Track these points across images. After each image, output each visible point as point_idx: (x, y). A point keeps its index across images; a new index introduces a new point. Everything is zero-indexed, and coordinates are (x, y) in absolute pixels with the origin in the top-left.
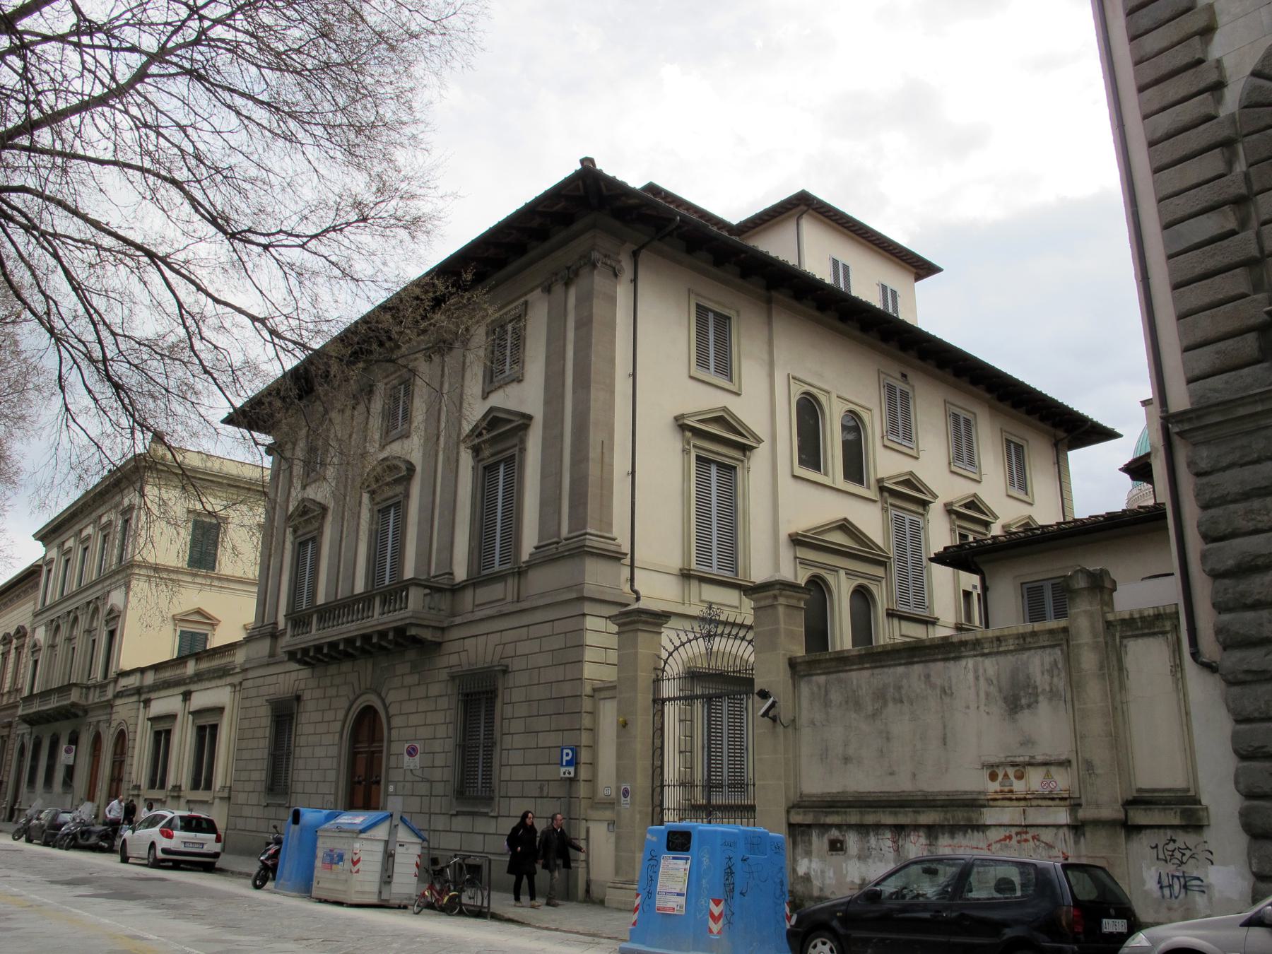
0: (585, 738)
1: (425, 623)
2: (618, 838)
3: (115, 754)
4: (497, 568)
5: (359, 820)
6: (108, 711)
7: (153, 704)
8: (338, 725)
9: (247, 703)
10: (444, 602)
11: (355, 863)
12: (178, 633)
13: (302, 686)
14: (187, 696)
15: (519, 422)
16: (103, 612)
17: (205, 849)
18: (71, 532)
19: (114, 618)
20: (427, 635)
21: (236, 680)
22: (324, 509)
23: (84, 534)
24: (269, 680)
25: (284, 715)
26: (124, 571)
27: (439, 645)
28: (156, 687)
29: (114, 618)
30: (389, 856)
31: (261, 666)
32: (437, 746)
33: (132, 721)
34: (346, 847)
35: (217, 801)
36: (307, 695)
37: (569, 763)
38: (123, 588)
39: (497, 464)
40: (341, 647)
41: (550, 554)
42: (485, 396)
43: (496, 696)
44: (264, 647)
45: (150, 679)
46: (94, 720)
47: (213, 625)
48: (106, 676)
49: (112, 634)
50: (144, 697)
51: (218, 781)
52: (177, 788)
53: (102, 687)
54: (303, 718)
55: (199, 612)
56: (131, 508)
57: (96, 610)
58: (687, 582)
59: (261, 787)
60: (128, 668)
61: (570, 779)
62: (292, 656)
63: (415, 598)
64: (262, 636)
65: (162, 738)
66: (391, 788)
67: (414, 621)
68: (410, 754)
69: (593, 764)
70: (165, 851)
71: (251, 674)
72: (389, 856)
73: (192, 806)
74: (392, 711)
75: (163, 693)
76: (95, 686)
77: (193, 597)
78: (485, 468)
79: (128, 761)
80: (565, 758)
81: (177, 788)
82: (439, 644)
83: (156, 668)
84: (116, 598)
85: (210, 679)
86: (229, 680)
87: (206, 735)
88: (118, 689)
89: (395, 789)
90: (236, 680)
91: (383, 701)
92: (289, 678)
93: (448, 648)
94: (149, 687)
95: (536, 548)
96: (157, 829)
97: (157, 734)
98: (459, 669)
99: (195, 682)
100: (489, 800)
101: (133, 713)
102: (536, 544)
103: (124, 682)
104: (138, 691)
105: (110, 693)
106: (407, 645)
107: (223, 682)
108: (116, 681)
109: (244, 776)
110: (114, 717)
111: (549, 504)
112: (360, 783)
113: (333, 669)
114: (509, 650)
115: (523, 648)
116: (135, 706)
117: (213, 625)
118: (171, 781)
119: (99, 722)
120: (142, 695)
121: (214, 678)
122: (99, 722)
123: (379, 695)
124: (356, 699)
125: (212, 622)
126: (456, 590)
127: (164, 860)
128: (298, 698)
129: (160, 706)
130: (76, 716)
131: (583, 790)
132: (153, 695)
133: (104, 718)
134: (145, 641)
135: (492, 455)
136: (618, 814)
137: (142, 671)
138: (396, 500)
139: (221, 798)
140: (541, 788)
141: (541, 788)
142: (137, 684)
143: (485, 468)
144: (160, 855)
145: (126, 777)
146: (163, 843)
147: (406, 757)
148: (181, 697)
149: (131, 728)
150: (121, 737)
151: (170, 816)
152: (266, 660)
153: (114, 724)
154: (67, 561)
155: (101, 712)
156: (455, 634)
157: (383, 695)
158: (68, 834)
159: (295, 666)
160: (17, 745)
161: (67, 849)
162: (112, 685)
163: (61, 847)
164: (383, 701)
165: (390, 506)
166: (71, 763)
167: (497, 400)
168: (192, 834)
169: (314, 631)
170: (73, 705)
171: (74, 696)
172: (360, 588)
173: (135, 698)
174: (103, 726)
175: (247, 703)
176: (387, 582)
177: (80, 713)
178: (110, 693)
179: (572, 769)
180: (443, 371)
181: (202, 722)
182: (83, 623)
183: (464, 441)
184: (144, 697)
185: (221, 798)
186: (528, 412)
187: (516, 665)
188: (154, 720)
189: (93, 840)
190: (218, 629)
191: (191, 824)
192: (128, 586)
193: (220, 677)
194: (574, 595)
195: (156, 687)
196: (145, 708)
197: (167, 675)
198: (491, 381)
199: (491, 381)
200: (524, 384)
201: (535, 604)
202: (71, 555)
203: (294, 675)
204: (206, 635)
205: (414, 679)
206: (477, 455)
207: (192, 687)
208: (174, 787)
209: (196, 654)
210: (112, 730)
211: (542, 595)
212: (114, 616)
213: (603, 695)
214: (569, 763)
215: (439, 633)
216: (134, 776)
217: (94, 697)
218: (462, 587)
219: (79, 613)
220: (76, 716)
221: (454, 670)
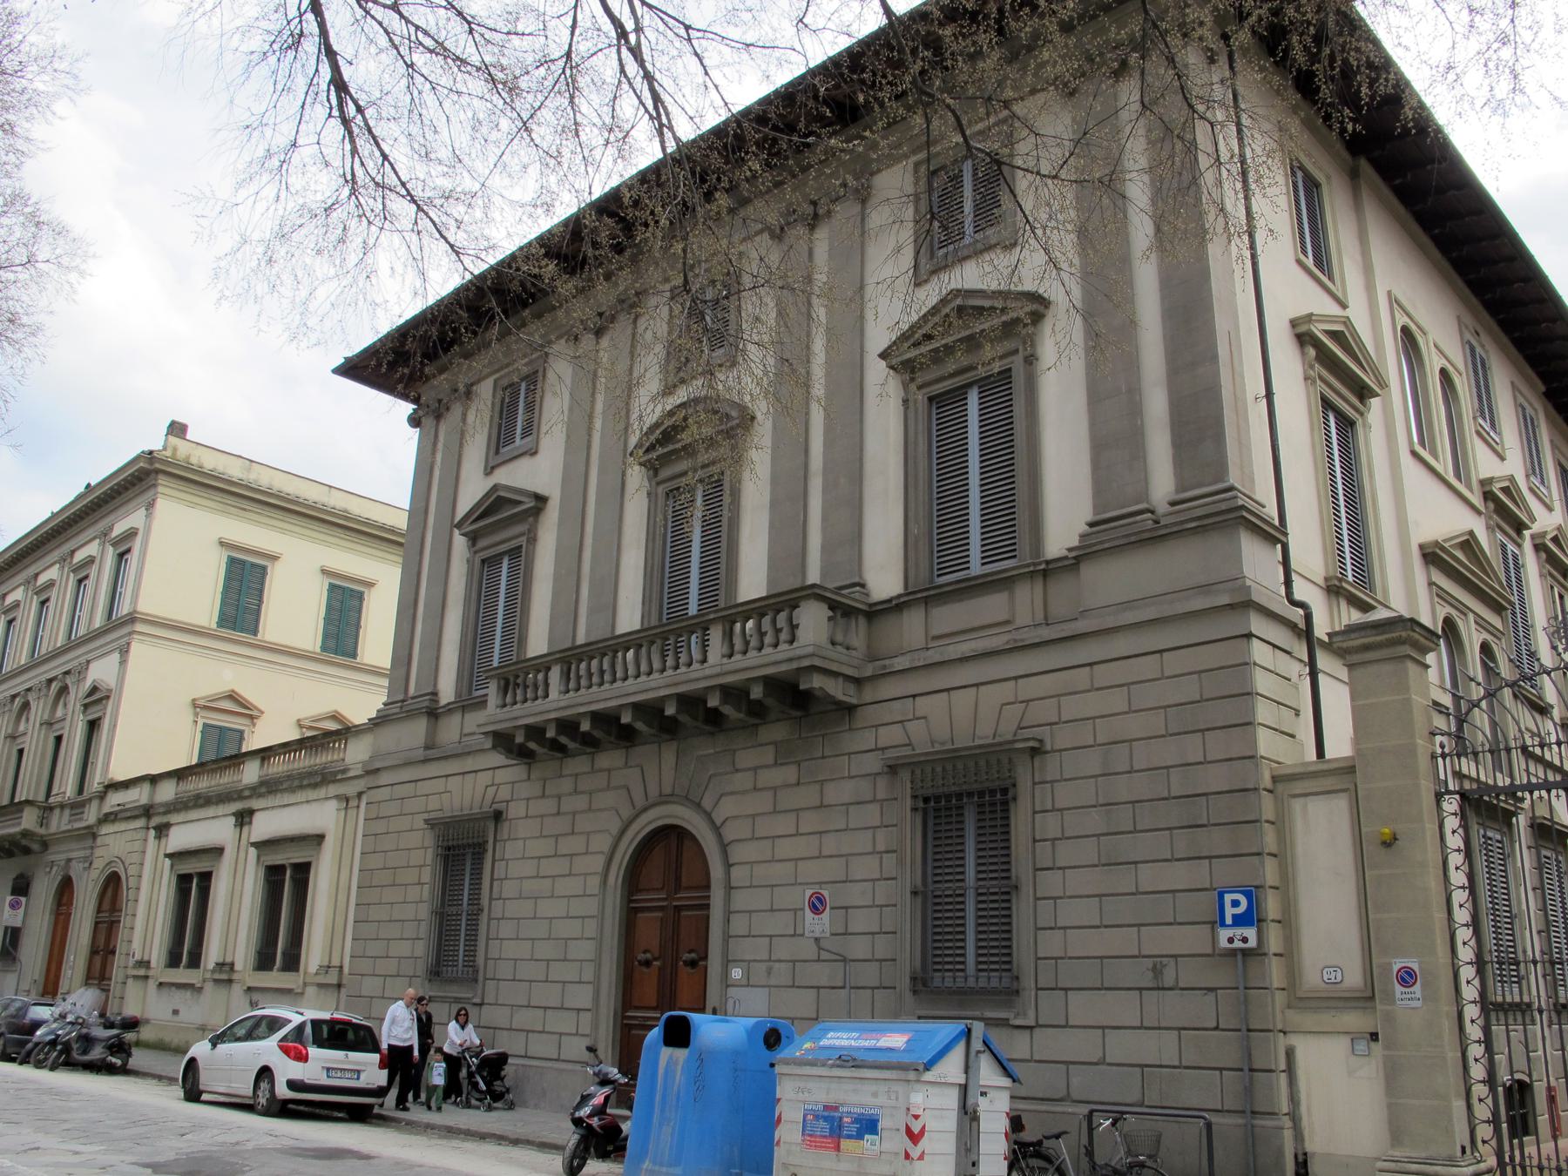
0: (1270, 872)
1: (834, 667)
2: (1392, 1075)
3: (99, 910)
4: (976, 568)
5: (895, 1040)
6: (89, 842)
7: (173, 831)
8: (598, 863)
9: (380, 827)
10: (858, 635)
11: (914, 1137)
12: (200, 727)
13: (504, 793)
14: (243, 818)
15: (530, 504)
16: (77, 694)
17: (363, 1082)
18: (56, 555)
19: (100, 700)
20: (836, 689)
21: (350, 789)
22: (748, 419)
23: (42, 579)
24: (425, 787)
25: (463, 849)
26: (120, 626)
27: (848, 710)
28: (179, 806)
29: (100, 700)
30: (968, 1115)
31: (408, 764)
32: (856, 895)
33: (135, 858)
34: (882, 1100)
35: (311, 990)
36: (515, 810)
37: (1239, 921)
38: (116, 656)
39: (959, 394)
40: (550, 734)
41: (1120, 531)
42: (489, 470)
43: (485, 851)
44: (414, 733)
45: (167, 792)
46: (60, 858)
47: (252, 717)
48: (81, 791)
49: (93, 726)
50: (156, 821)
51: (314, 954)
52: (226, 966)
53: (77, 807)
54: (511, 850)
55: (232, 697)
56: (131, 534)
57: (64, 690)
58: (1333, 598)
59: (421, 968)
60: (121, 777)
61: (1246, 953)
62: (502, 741)
63: (813, 622)
64: (410, 715)
65: (193, 885)
66: (737, 973)
67: (817, 662)
68: (815, 910)
69: (1288, 921)
70: (292, 1085)
71: (385, 778)
72: (968, 1115)
73: (256, 996)
74: (729, 833)
75: (193, 814)
76: (62, 806)
77: (225, 672)
78: (483, 561)
79: (125, 921)
80: (1229, 912)
81: (226, 966)
82: (850, 709)
83: (179, 775)
84: (102, 671)
85: (292, 790)
86: (333, 790)
87: (286, 880)
88: (106, 809)
89: (747, 974)
90: (350, 789)
91: (708, 816)
92: (482, 781)
93: (868, 715)
94: (166, 804)
95: (1091, 525)
96: (272, 1042)
97: (184, 881)
98: (907, 751)
99: (261, 796)
100: (1010, 994)
101: (137, 846)
102: (1089, 517)
103: (115, 799)
104: (147, 811)
105: (91, 815)
106: (793, 706)
107: (322, 792)
108: (102, 796)
109: (375, 948)
110: (98, 852)
111: (1114, 444)
112: (647, 963)
113: (578, 764)
114: (1042, 712)
115: (1073, 707)
116: (141, 834)
117: (252, 717)
118: (213, 953)
119: (69, 860)
120: (155, 818)
121: (301, 787)
122: (69, 860)
123: (698, 806)
124: (645, 810)
125: (250, 713)
126: (876, 613)
127: (286, 1102)
128: (498, 816)
129: (187, 834)
130: (27, 851)
131: (1275, 973)
132: (173, 818)
133: (82, 854)
134: (149, 734)
135: (684, 474)
136: (1389, 1018)
137: (153, 780)
138: (513, 544)
139: (320, 986)
140: (1157, 971)
141: (1157, 971)
142: (144, 800)
143: (483, 561)
144: (283, 1091)
145: (121, 948)
146: (287, 1070)
147: (808, 914)
148: (232, 820)
149: (132, 870)
150: (113, 883)
151: (297, 1020)
152: (420, 754)
153: (99, 864)
154: (10, 622)
155: (74, 845)
156: (889, 689)
157: (707, 803)
158: (53, 1043)
159: (498, 759)
160: (55, 878)
161: (53, 1068)
162: (95, 804)
163: (39, 1065)
164: (708, 816)
165: (502, 554)
166: (19, 924)
167: (504, 476)
168: (340, 1054)
169: (554, 693)
170: (26, 834)
171: (29, 820)
172: (629, 619)
173: (140, 823)
174: (76, 871)
175: (380, 827)
176: (495, 664)
177: (35, 847)
178: (91, 815)
179: (1251, 933)
180: (436, 436)
181: (277, 859)
182: (39, 710)
183: (459, 526)
184: (156, 821)
185: (320, 986)
186: (539, 491)
187: (1061, 738)
188: (263, 846)
189: (97, 1053)
190: (259, 723)
191: (337, 1035)
192: (124, 651)
193: (315, 786)
194: (1225, 600)
195: (179, 806)
196: (159, 837)
197: (202, 784)
198: (497, 452)
199: (497, 452)
200: (538, 456)
201: (1110, 622)
202: (19, 614)
203: (484, 778)
204: (242, 732)
205: (788, 773)
206: (474, 545)
207: (255, 804)
208: (220, 966)
209: (223, 763)
210: (94, 874)
211: (1128, 605)
212: (98, 698)
213: (1299, 787)
214: (1239, 921)
215: (851, 689)
216: (136, 945)
217: (60, 823)
218: (894, 607)
219: (31, 697)
220: (27, 851)
221: (433, 815)
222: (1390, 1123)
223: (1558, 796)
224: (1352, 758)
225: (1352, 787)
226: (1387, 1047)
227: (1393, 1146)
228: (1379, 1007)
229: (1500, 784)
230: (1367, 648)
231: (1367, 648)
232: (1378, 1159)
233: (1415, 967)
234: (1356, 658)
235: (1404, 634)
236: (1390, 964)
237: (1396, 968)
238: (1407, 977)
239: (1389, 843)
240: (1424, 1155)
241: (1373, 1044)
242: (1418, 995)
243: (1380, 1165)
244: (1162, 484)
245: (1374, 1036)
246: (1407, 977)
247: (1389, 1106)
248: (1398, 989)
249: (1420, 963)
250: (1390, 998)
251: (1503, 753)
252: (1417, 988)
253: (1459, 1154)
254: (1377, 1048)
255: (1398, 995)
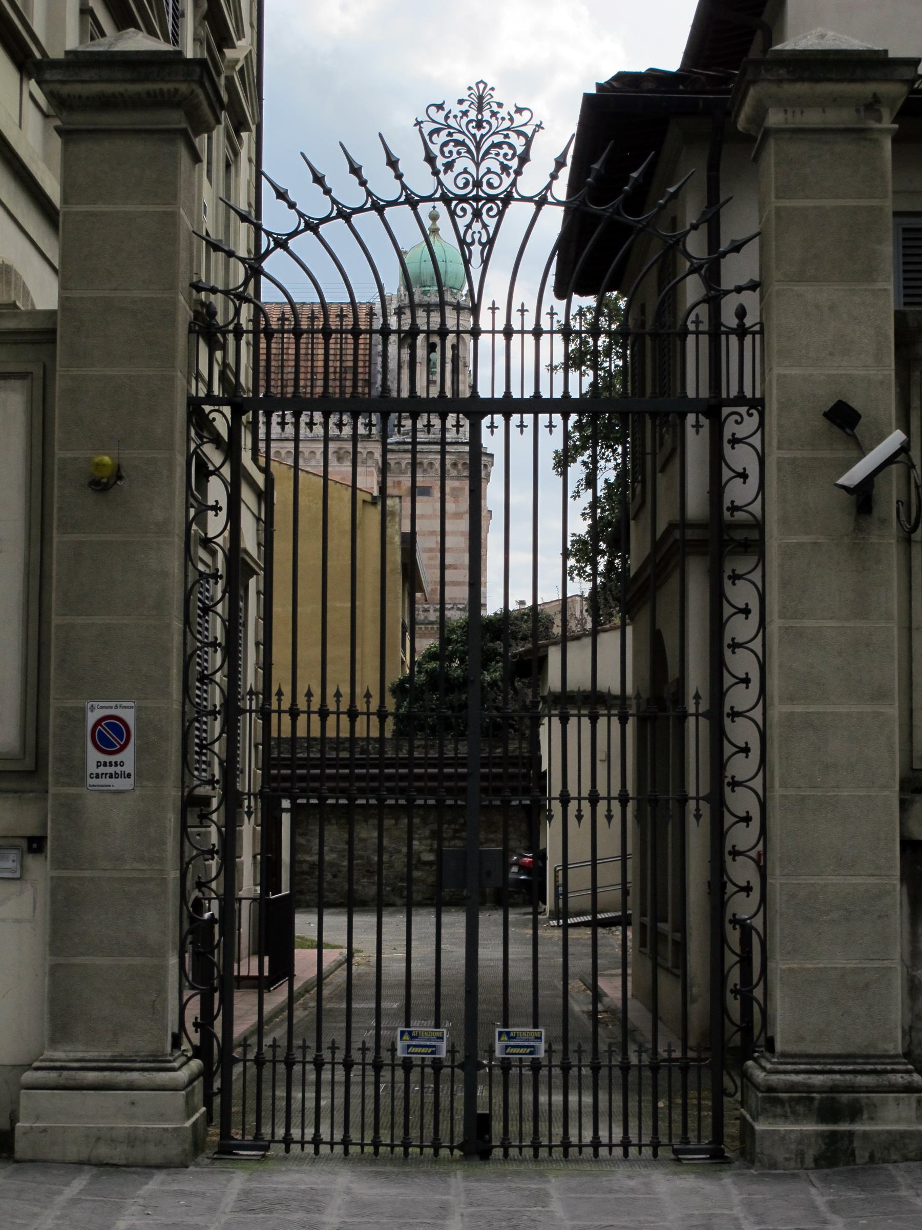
136: (71, 810)
222: (53, 1001)
223: (697, 426)
224: (53, 313)
225: (38, 372)
226: (59, 864)
227: (54, 1041)
228: (52, 790)
229: (331, 733)
230: (106, 103)
231: (106, 103)
232: (29, 1067)
233: (129, 716)
234: (80, 120)
235: (183, 88)
236: (83, 710)
237: (92, 718)
238: (111, 736)
239: (103, 484)
240: (109, 1054)
241: (32, 862)
242: (129, 767)
243: (29, 1076)
244: (389, 447)
245: (36, 844)
246: (111, 736)
247: (54, 970)
248: (93, 756)
249: (138, 710)
250: (75, 771)
251: (274, 716)
252: (128, 756)
253: (169, 1048)
254: (40, 869)
255: (91, 768)
